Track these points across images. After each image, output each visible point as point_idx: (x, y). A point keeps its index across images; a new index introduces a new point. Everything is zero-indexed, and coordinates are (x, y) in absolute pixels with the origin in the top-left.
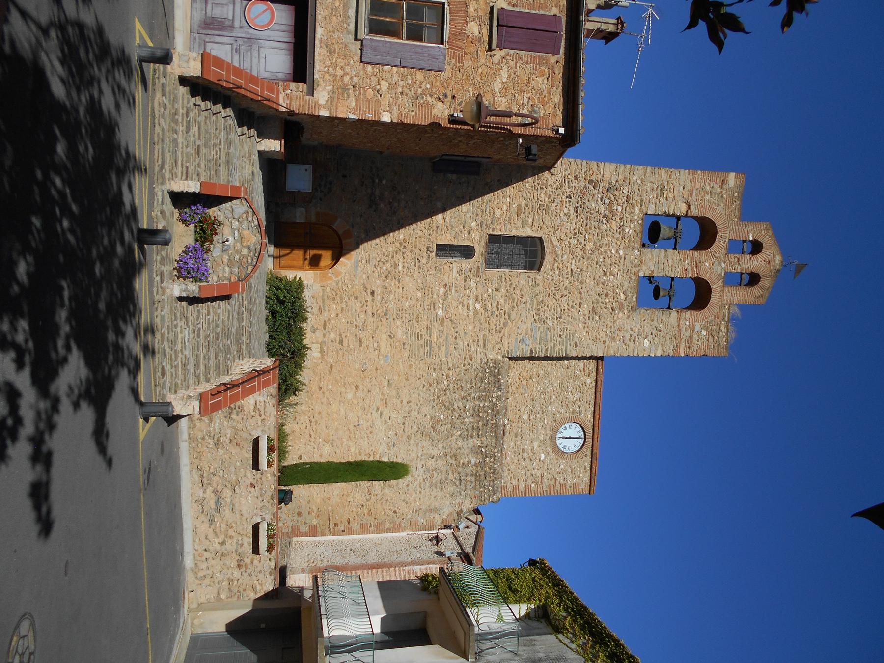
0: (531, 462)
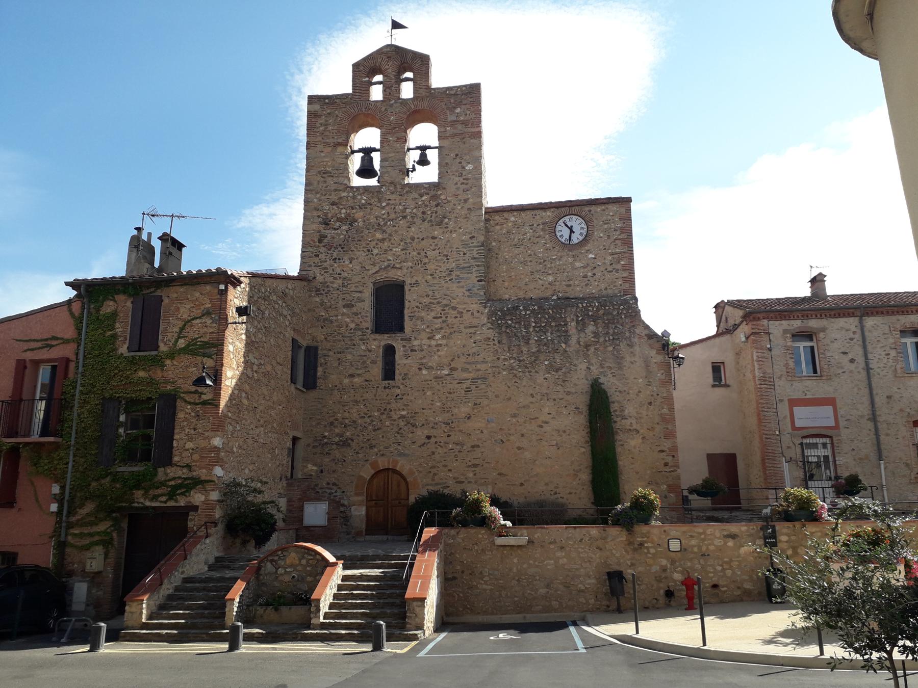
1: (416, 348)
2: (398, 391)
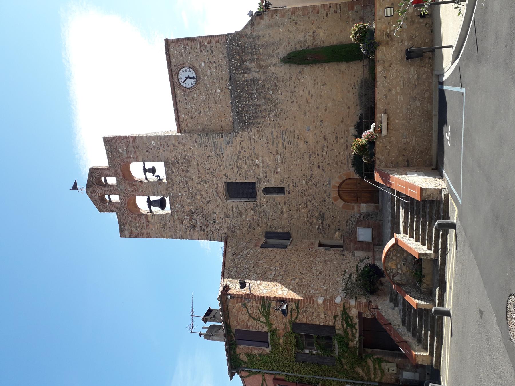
1: (265, 175)
2: (291, 185)
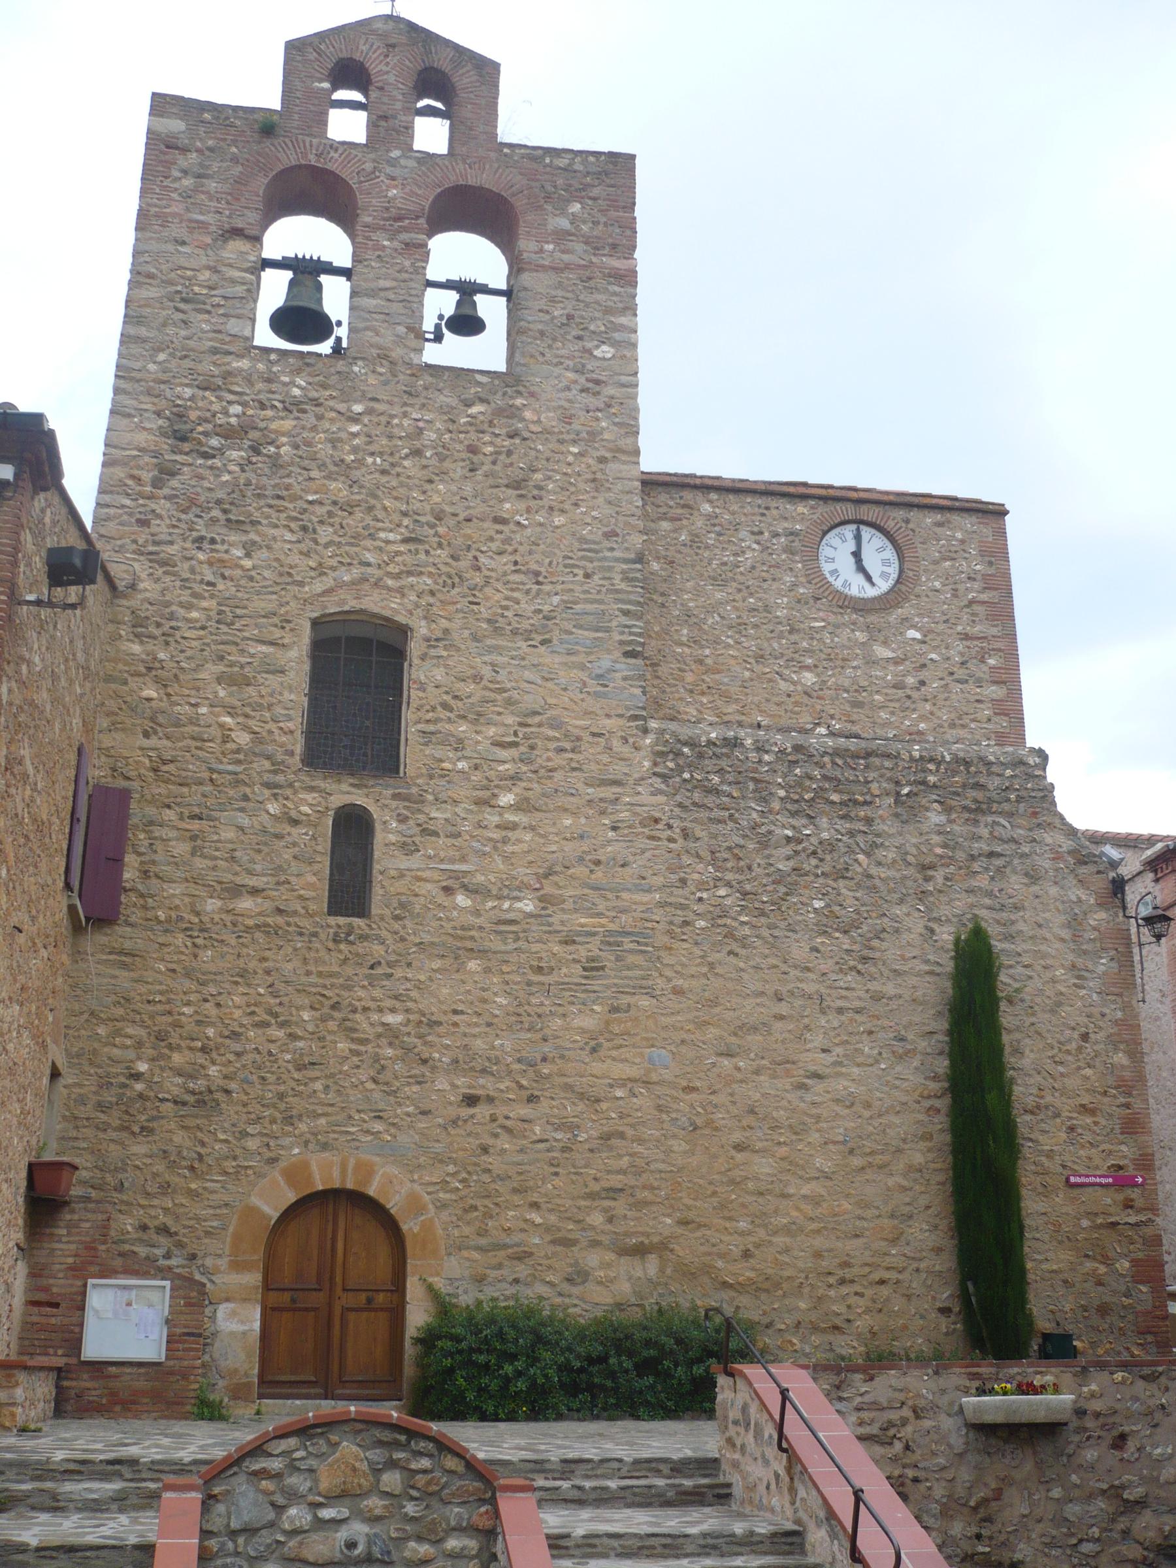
0: (931, 666)
2: (378, 950)
